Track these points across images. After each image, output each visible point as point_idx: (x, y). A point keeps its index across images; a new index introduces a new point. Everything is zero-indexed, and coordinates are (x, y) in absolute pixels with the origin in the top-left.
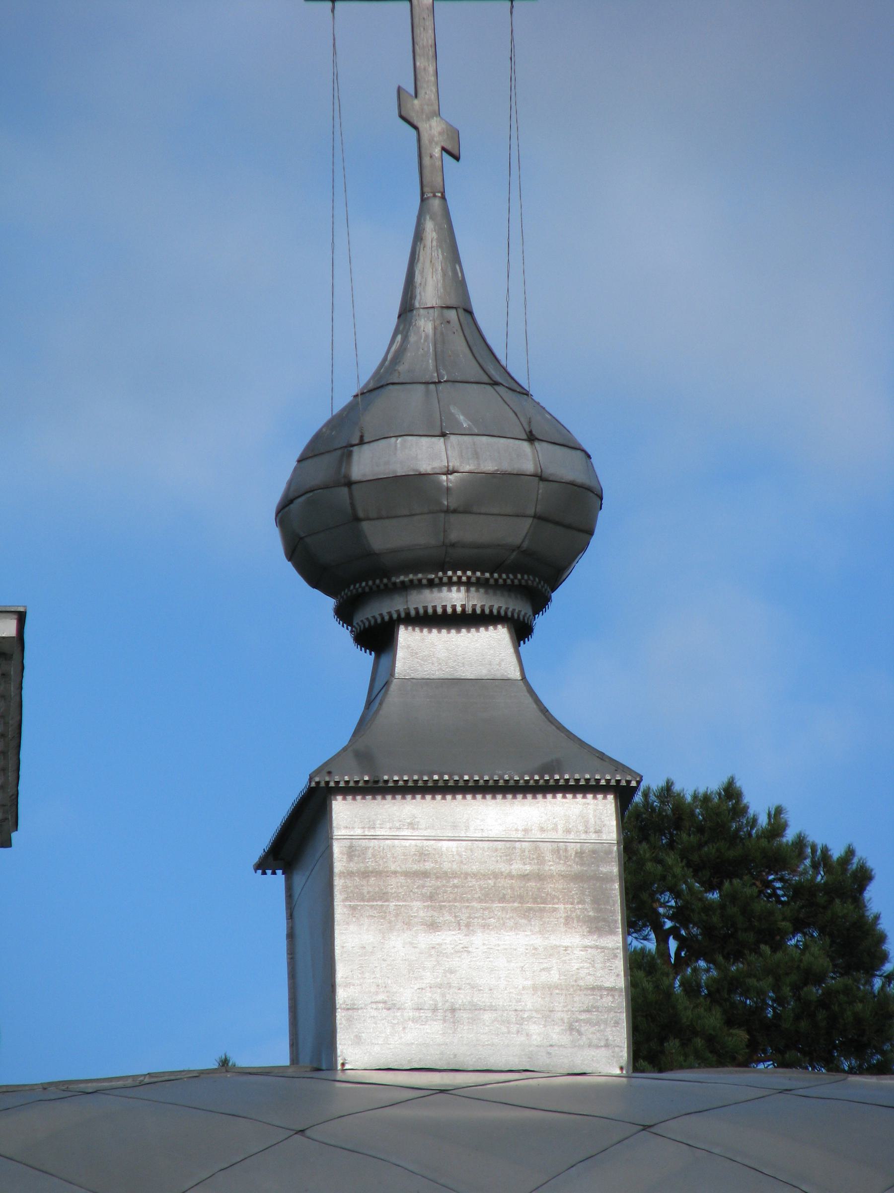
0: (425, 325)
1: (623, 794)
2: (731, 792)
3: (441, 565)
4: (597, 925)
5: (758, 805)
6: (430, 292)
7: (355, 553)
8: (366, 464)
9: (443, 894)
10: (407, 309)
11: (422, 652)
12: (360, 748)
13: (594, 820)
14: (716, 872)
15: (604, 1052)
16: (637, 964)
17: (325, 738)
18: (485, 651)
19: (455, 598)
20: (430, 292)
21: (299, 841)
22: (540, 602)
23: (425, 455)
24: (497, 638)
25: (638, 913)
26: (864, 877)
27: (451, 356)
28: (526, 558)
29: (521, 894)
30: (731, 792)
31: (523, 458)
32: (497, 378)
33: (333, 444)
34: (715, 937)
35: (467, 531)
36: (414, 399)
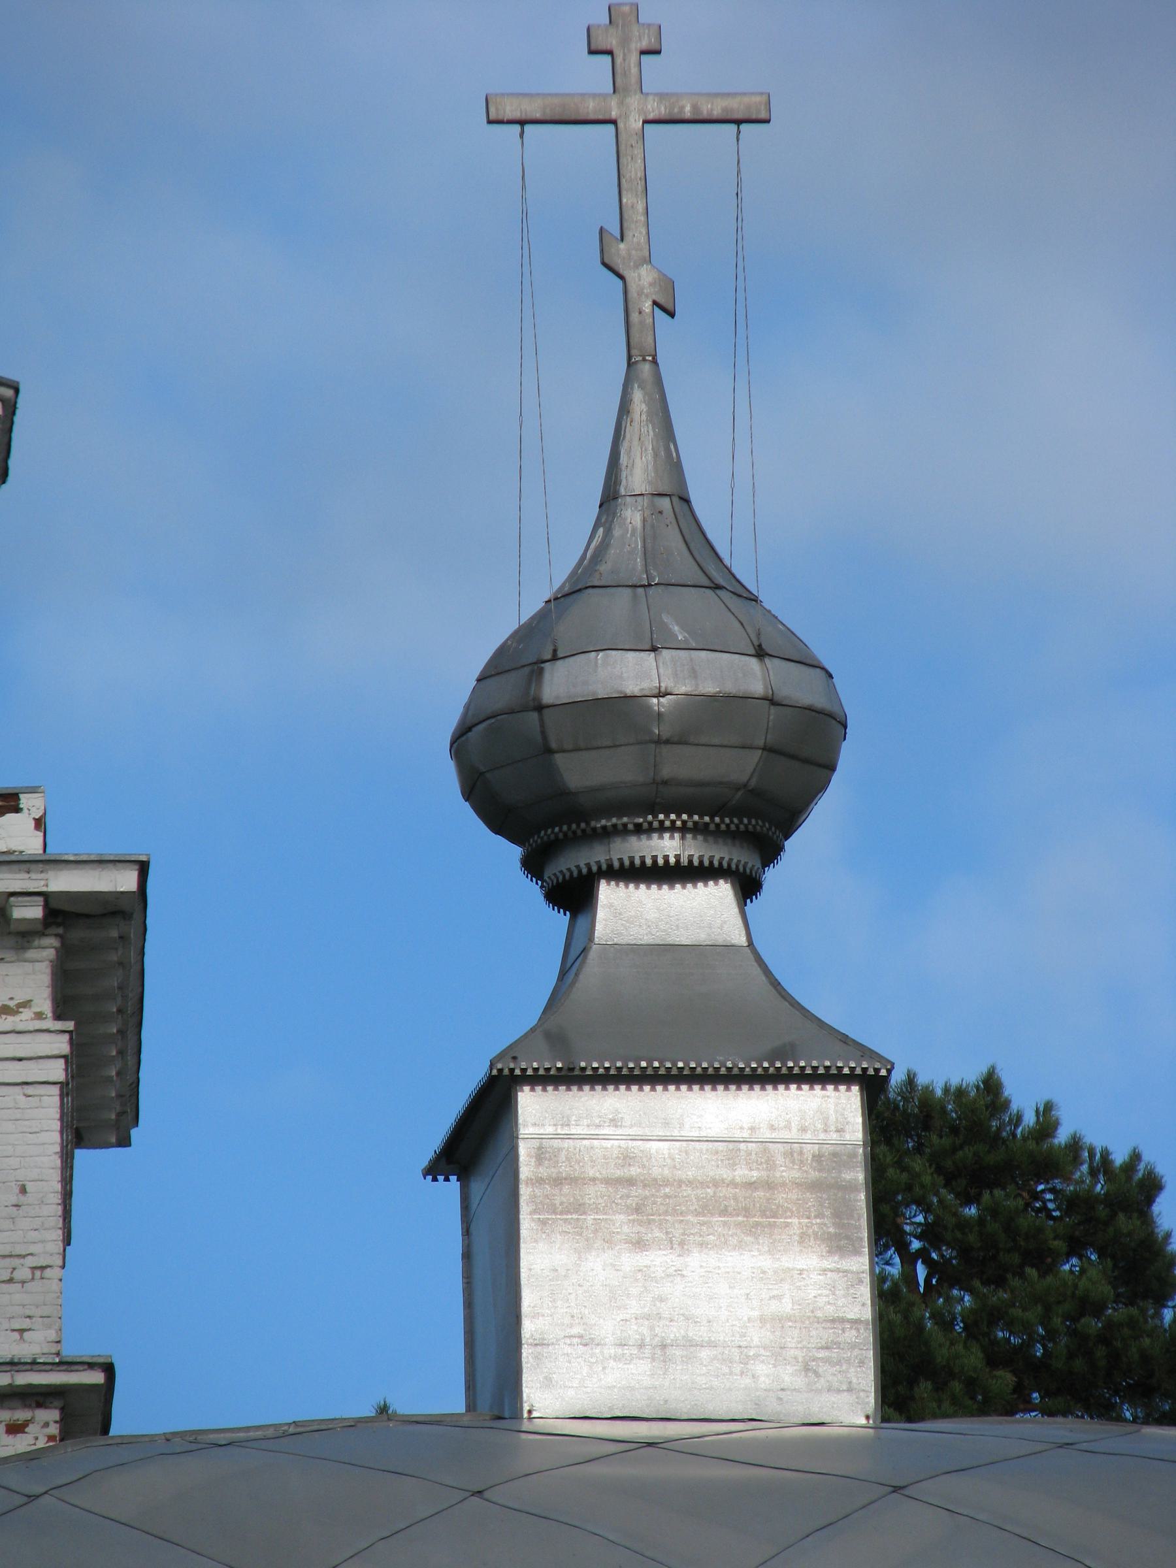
0: (632, 516)
1: (873, 1086)
2: (991, 1085)
3: (651, 806)
4: (838, 1244)
5: (1023, 1100)
6: (639, 474)
7: (547, 792)
8: (560, 684)
9: (651, 1204)
10: (610, 497)
11: (622, 911)
12: (552, 1028)
13: (833, 1116)
14: (973, 1180)
15: (846, 1398)
16: (888, 1297)
17: (510, 1013)
18: (702, 912)
19: (668, 847)
20: (639, 474)
21: (476, 1143)
22: (770, 852)
23: (631, 673)
24: (721, 893)
25: (885, 1232)
26: (1152, 1186)
27: (662, 555)
28: (749, 817)
29: (744, 1205)
30: (991, 1085)
31: (750, 677)
32: (719, 581)
33: (521, 659)
34: (976, 1259)
35: (682, 766)
36: (616, 607)
